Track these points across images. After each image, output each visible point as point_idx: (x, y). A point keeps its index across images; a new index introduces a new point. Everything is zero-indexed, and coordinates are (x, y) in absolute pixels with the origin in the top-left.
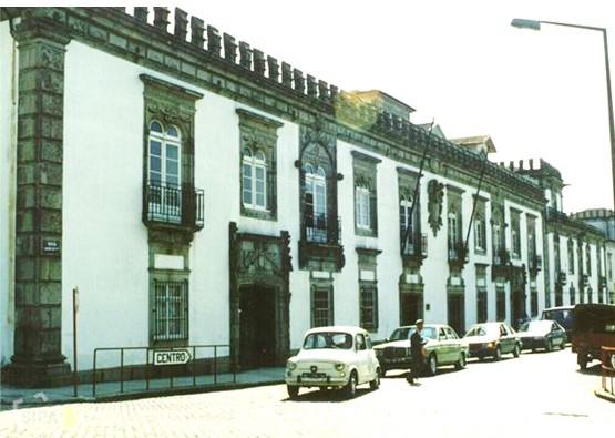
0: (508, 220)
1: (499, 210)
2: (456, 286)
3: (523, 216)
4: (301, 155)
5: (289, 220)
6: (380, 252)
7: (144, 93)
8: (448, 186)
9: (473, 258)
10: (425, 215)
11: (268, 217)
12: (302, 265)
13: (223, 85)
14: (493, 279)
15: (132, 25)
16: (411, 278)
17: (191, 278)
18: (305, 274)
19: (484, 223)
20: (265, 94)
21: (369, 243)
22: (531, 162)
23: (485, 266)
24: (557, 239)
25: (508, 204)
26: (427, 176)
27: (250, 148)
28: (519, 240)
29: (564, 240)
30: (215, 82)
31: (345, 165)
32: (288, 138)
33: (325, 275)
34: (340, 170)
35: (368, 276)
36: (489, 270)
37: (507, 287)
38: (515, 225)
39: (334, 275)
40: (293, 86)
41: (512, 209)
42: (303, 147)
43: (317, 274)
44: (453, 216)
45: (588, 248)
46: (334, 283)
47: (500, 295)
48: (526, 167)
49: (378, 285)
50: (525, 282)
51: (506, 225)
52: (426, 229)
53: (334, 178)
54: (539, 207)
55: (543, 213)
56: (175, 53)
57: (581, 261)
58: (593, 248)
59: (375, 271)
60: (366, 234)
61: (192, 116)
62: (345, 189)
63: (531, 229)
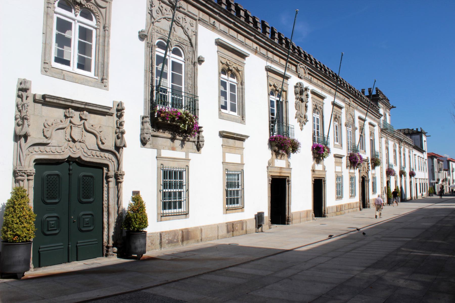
0: (357, 125)
3: (367, 123)
6: (247, 137)
8: (313, 93)
13: (258, 50)
16: (319, 167)
17: (245, 168)
18: (149, 153)
23: (341, 157)
33: (179, 154)
34: (200, 53)
38: (362, 130)
43: (166, 153)
44: (318, 116)
45: (404, 150)
46: (191, 164)
55: (379, 124)
58: (407, 150)
63: (372, 134)
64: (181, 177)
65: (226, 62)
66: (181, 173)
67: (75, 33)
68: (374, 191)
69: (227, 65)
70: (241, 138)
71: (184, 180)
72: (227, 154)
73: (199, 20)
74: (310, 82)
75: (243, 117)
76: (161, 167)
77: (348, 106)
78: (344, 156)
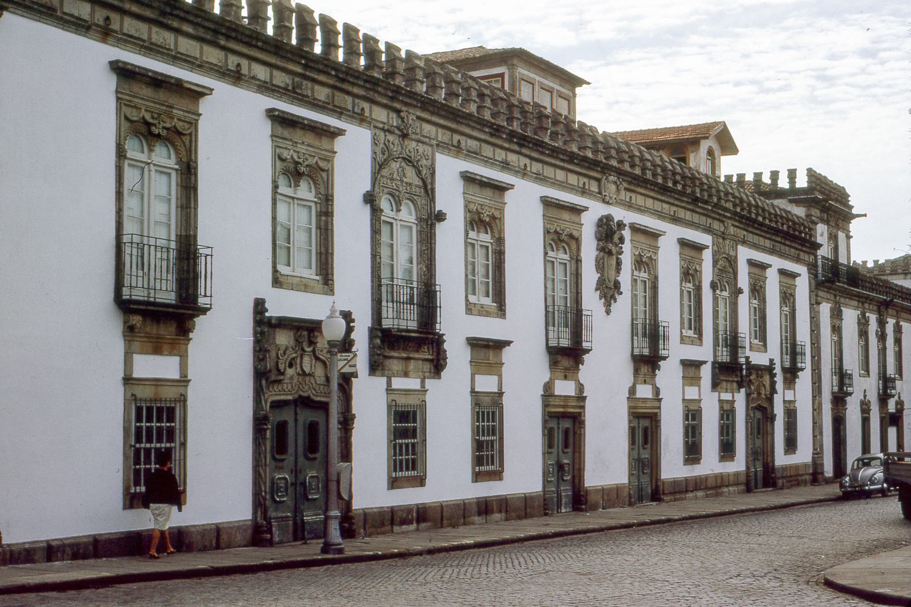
0: (743, 281)
1: (726, 269)
2: (645, 400)
4: (373, 185)
5: (353, 291)
6: (508, 343)
7: (117, 92)
8: (636, 229)
9: (676, 351)
10: (590, 277)
11: (320, 286)
12: (375, 367)
13: (245, 71)
14: (715, 385)
15: (272, 50)
17: (702, 405)
18: (380, 382)
19: (698, 288)
20: (314, 80)
21: (489, 328)
22: (792, 174)
24: (837, 314)
25: (744, 254)
26: (595, 210)
27: (292, 171)
28: (763, 318)
29: (850, 316)
30: (232, 67)
31: (450, 197)
32: (354, 153)
33: (413, 383)
35: (487, 384)
36: (706, 372)
37: (740, 399)
38: (757, 290)
39: (429, 383)
40: (270, 31)
41: (751, 263)
42: (379, 167)
43: (399, 383)
46: (429, 398)
47: (727, 414)
48: (783, 183)
49: (505, 400)
50: (773, 391)
51: (740, 291)
52: (591, 301)
53: (431, 220)
54: (805, 257)
55: (812, 268)
56: (165, 21)
57: (883, 351)
59: (500, 376)
60: (483, 312)
61: (194, 124)
62: (451, 239)
63: (787, 297)
64: (171, 419)
65: (292, 157)
66: (415, 413)
67: (149, 187)
68: (791, 444)
69: (479, 213)
70: (499, 345)
71: (177, 424)
72: (686, 388)
73: (438, 145)
74: (630, 206)
75: (765, 345)
76: (131, 399)
77: (721, 240)
78: (705, 362)
